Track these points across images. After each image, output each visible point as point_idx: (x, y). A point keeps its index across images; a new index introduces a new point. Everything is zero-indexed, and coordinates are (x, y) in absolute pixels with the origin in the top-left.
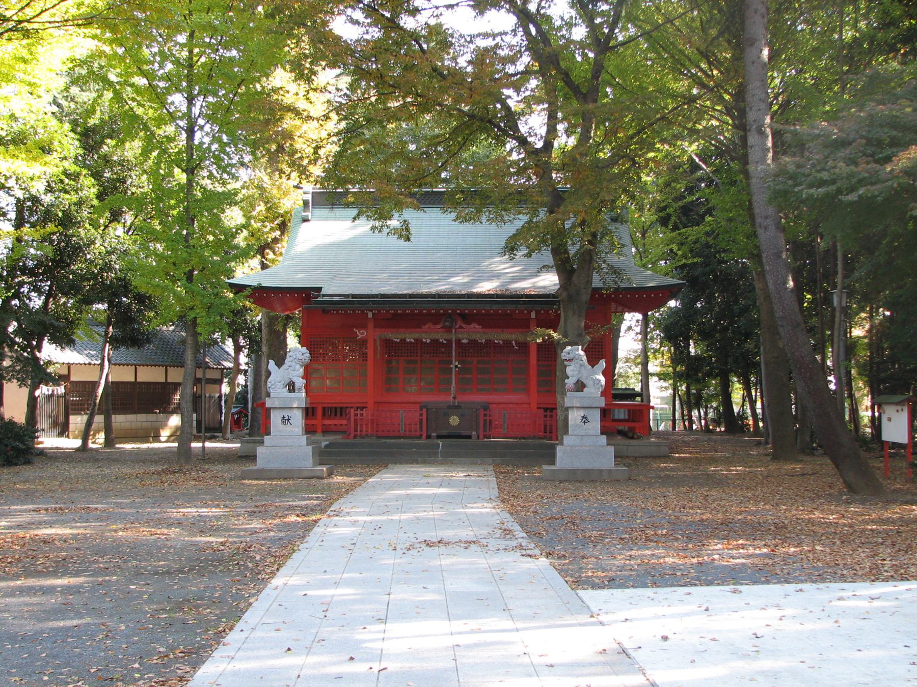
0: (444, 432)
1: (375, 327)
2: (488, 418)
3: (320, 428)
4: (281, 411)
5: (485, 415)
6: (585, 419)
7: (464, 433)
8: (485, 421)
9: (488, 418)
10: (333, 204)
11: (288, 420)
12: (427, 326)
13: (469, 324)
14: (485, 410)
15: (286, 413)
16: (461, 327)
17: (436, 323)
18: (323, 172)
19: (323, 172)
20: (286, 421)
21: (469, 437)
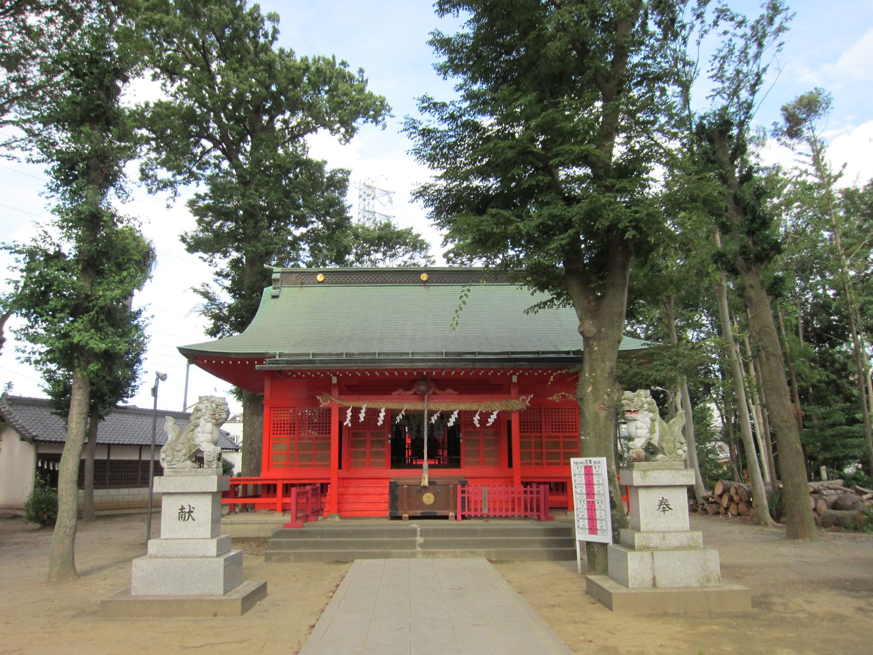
0: (418, 513)
1: (340, 394)
2: (466, 495)
3: (279, 507)
4: (178, 497)
5: (463, 492)
6: (664, 506)
7: (439, 513)
8: (463, 498)
9: (466, 495)
10: (302, 284)
11: (190, 512)
12: (397, 392)
13: (444, 390)
14: (463, 486)
15: (186, 502)
16: (434, 393)
17: (407, 389)
18: (282, 51)
19: (282, 51)
20: (185, 514)
21: (446, 517)
